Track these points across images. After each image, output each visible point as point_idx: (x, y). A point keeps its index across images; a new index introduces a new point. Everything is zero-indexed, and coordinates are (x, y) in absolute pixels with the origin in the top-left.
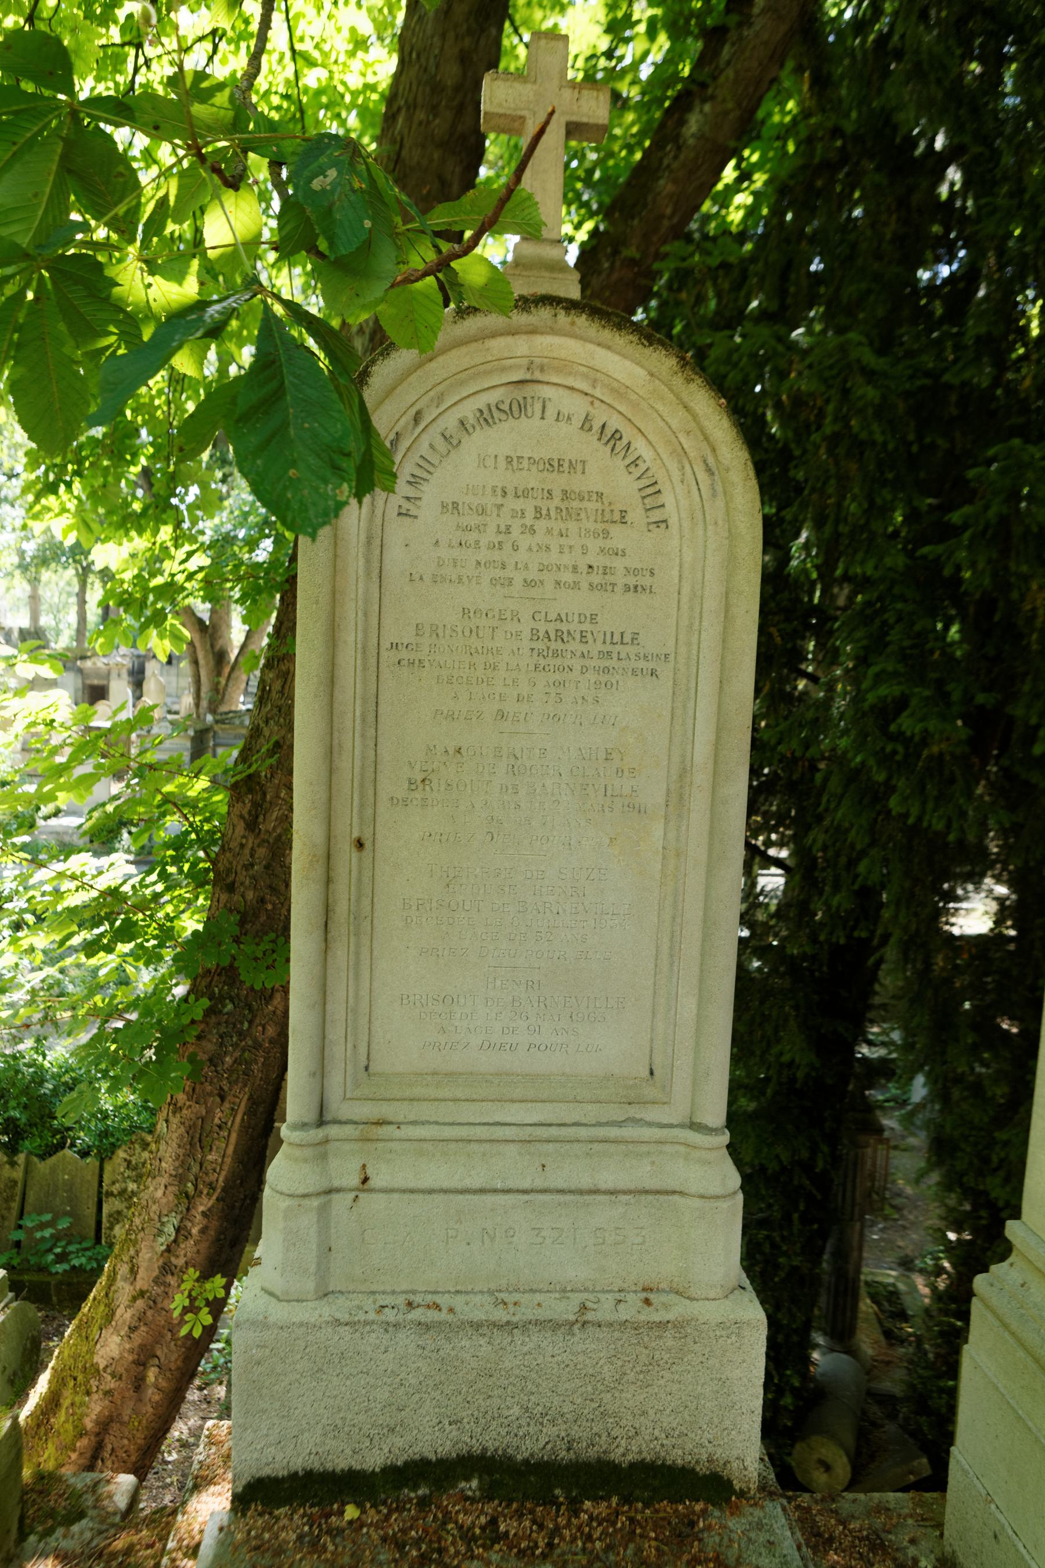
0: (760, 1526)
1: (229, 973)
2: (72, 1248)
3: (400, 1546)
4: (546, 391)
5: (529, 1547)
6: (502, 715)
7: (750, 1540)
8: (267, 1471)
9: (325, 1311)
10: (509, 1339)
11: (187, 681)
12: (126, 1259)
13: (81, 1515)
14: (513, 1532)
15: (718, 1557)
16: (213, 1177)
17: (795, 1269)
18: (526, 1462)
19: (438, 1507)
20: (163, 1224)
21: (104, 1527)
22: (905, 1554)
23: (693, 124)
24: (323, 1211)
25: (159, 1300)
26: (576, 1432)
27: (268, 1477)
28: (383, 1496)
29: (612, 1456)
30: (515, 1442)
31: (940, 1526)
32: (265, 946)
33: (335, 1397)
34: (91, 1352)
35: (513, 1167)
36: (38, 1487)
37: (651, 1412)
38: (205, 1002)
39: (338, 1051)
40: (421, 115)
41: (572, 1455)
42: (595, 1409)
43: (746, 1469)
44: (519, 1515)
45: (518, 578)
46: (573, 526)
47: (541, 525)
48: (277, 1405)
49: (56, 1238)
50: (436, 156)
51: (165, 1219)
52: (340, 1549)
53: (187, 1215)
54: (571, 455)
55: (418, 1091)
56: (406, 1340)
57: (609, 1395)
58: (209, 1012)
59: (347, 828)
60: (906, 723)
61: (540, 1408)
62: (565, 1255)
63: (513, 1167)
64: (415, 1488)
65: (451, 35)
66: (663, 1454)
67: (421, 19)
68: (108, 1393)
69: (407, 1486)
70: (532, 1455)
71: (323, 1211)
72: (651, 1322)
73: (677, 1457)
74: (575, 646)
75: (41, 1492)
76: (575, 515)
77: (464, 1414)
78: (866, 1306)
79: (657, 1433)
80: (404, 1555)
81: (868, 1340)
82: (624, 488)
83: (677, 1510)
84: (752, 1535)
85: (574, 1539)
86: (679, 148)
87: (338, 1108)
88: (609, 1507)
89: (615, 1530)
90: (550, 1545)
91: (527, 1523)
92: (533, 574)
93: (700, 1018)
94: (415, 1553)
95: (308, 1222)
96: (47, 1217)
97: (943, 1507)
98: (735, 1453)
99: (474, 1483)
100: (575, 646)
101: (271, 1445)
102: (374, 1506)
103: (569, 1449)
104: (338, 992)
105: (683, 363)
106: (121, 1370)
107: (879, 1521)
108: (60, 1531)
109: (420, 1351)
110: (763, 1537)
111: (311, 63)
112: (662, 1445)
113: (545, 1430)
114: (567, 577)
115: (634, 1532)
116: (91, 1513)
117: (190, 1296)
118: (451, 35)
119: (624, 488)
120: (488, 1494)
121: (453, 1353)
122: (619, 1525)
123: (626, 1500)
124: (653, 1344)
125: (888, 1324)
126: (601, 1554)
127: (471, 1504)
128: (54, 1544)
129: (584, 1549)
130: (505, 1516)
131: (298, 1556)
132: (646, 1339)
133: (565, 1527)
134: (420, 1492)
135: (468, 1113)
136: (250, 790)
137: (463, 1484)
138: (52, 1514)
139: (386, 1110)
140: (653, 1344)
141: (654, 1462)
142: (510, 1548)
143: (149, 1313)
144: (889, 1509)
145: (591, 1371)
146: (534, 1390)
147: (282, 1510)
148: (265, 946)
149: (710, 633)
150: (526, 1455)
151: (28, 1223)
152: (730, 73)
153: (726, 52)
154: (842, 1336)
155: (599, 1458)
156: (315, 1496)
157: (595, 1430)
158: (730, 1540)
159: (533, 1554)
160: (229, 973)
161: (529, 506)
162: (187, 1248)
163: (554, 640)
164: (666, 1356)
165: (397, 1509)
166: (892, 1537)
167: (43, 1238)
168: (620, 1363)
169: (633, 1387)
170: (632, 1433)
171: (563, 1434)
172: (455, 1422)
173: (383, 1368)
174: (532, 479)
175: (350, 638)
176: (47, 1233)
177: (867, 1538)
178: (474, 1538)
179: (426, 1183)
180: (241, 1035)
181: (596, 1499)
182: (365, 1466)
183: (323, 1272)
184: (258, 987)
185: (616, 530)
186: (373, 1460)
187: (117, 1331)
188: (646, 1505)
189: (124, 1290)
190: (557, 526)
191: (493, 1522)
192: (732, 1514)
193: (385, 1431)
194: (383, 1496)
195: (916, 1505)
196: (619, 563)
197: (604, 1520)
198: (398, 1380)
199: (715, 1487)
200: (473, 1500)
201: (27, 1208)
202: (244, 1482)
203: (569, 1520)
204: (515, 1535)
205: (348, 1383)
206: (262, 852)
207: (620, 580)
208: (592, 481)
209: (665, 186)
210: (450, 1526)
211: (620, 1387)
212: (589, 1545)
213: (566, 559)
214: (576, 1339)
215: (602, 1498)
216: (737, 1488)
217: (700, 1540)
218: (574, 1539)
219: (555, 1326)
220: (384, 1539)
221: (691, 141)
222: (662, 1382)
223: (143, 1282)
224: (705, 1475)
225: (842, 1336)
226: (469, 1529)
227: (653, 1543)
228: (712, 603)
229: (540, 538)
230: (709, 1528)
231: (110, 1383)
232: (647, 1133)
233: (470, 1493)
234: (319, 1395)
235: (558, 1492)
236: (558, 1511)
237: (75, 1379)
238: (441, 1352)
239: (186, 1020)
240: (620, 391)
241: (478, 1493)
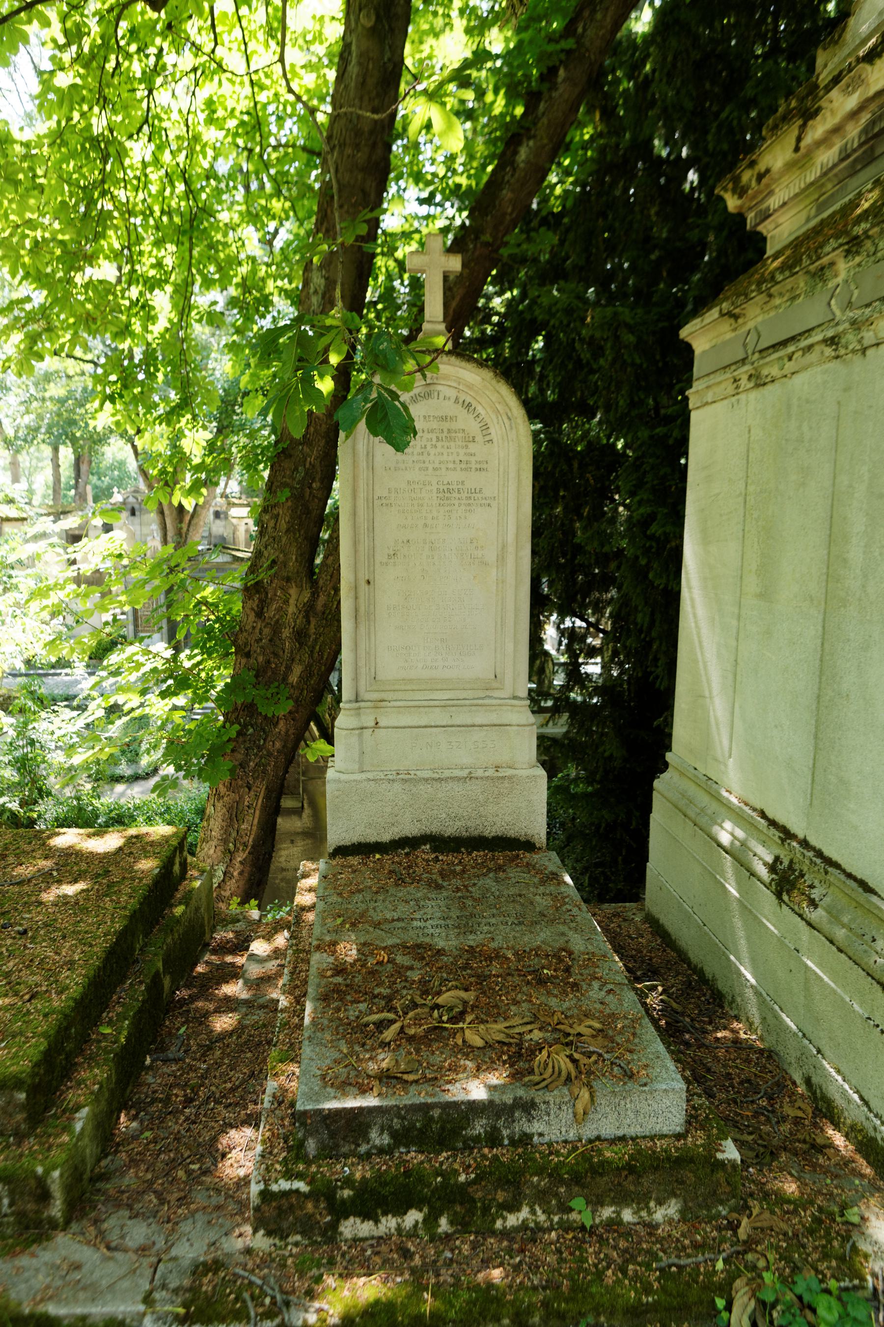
1: (250, 708)
4: (439, 388)
6: (426, 525)
9: (364, 776)
11: (155, 527)
16: (246, 839)
23: (523, 154)
24: (360, 736)
26: (469, 824)
32: (272, 690)
35: (438, 717)
38: (237, 727)
39: (363, 671)
40: (348, 151)
45: (431, 467)
46: (452, 444)
47: (439, 444)
50: (359, 177)
53: (230, 864)
54: (450, 414)
55: (397, 687)
56: (397, 786)
58: (239, 733)
59: (363, 576)
60: (654, 529)
62: (461, 754)
63: (438, 717)
65: (366, 98)
67: (346, 87)
71: (360, 736)
72: (500, 779)
73: (512, 834)
74: (456, 495)
76: (451, 439)
82: (473, 427)
86: (514, 170)
87: (364, 695)
92: (437, 465)
93: (515, 651)
95: (354, 740)
100: (456, 495)
104: (362, 646)
105: (496, 375)
111: (262, 88)
114: (451, 466)
118: (366, 98)
119: (473, 427)
123: (493, 850)
135: (418, 696)
136: (258, 592)
139: (383, 695)
148: (272, 690)
149: (512, 488)
152: (545, 120)
153: (542, 106)
160: (250, 708)
161: (434, 436)
162: (232, 885)
163: (446, 493)
174: (434, 425)
175: (361, 495)
179: (402, 724)
180: (260, 748)
183: (361, 763)
184: (270, 715)
185: (471, 445)
186: (386, 838)
190: (446, 444)
196: (473, 459)
199: (529, 846)
206: (267, 631)
207: (474, 466)
208: (460, 425)
209: (506, 194)
213: (451, 458)
219: (458, 779)
221: (522, 165)
228: (512, 475)
229: (439, 449)
232: (494, 702)
239: (225, 738)
240: (470, 386)
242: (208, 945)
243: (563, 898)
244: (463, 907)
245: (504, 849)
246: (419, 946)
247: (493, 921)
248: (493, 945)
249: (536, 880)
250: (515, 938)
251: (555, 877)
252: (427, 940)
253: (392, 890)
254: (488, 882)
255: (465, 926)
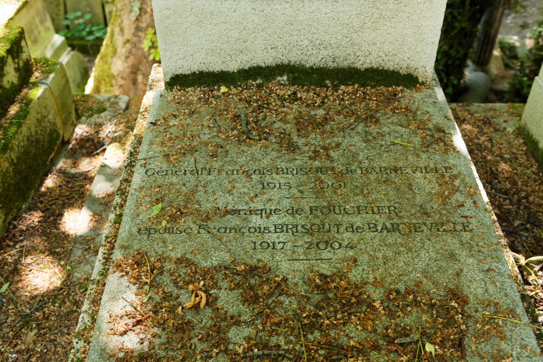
0: (430, 96)
2: (94, 28)
3: (249, 102)
5: (312, 103)
7: (424, 101)
8: (179, 72)
10: (302, 5)
12: (117, 24)
13: (104, 110)
14: (304, 97)
15: (407, 107)
17: (463, 29)
18: (311, 68)
19: (267, 88)
20: (132, 7)
21: (115, 114)
22: (501, 126)
25: (137, 44)
26: (337, 53)
27: (181, 74)
28: (239, 83)
29: (356, 65)
30: (306, 58)
31: (520, 116)
33: (210, 35)
34: (109, 68)
36: (83, 99)
37: (378, 43)
41: (335, 65)
42: (348, 42)
43: (426, 72)
44: (308, 91)
48: (181, 39)
49: (85, 24)
51: (133, 4)
52: (219, 103)
57: (356, 35)
61: (318, 41)
64: (255, 80)
66: (383, 64)
68: (121, 86)
69: (251, 79)
70: (314, 64)
73: (390, 66)
75: (84, 101)
77: (278, 44)
78: (496, 52)
79: (380, 54)
80: (250, 105)
81: (495, 67)
83: (388, 90)
84: (426, 100)
85: (335, 100)
88: (354, 88)
89: (356, 97)
90: (323, 103)
91: (312, 94)
94: (255, 105)
96: (79, 14)
97: (524, 109)
98: (421, 64)
99: (285, 78)
101: (180, 59)
102: (235, 87)
103: (334, 62)
106: (125, 76)
107: (489, 114)
108: (95, 116)
109: (253, 11)
110: (431, 100)
112: (383, 60)
113: (321, 52)
115: (365, 98)
116: (109, 109)
117: (151, 41)
120: (293, 82)
121: (271, 12)
122: (358, 95)
123: (363, 85)
124: (382, 7)
125: (507, 61)
126: (348, 106)
127: (284, 87)
128: (94, 120)
129: (339, 104)
130: (300, 92)
131: (199, 106)
132: (378, 4)
133: (330, 96)
134: (258, 82)
137: (279, 78)
138: (91, 109)
140: (382, 7)
141: (378, 68)
142: (302, 103)
143: (134, 50)
144: (495, 110)
145: (347, 22)
146: (316, 32)
147: (190, 89)
150: (311, 64)
151: (71, 16)
154: (482, 63)
155: (349, 66)
156: (205, 83)
157: (348, 52)
158: (414, 101)
159: (314, 106)
164: (389, 14)
165: (246, 88)
166: (495, 120)
167: (79, 24)
168: (363, 17)
169: (369, 30)
170: (367, 53)
171: (331, 54)
172: (274, 48)
173: (234, 20)
176: (81, 21)
177: (483, 120)
178: (285, 100)
181: (347, 85)
182: (229, 70)
186: (233, 67)
187: (119, 58)
188: (372, 87)
189: (119, 40)
191: (295, 93)
192: (416, 92)
193: (238, 52)
194: (239, 83)
195: (510, 108)
197: (350, 93)
198: (242, 26)
199: (410, 81)
200: (284, 85)
201: (68, 9)
202: (170, 77)
203: (333, 93)
204: (305, 98)
205: (216, 28)
210: (272, 95)
211: (362, 30)
212: (342, 102)
214: (339, 4)
215: (350, 85)
216: (420, 81)
217: (399, 101)
218: (335, 100)
220: (240, 100)
222: (385, 28)
223: (128, 34)
224: (404, 75)
225: (482, 63)
226: (282, 96)
227: (375, 102)
230: (404, 97)
231: (122, 82)
233: (283, 82)
234: (202, 34)
235: (327, 82)
236: (327, 90)
237: (104, 80)
238: (265, 12)
241: (287, 82)
242: (65, 143)
243: (454, 177)
244: (319, 192)
245: (378, 83)
246: (252, 270)
247: (357, 221)
248: (355, 275)
249: (417, 140)
250: (386, 259)
251: (439, 138)
252: (265, 256)
253: (233, 150)
254: (354, 141)
255: (319, 236)
